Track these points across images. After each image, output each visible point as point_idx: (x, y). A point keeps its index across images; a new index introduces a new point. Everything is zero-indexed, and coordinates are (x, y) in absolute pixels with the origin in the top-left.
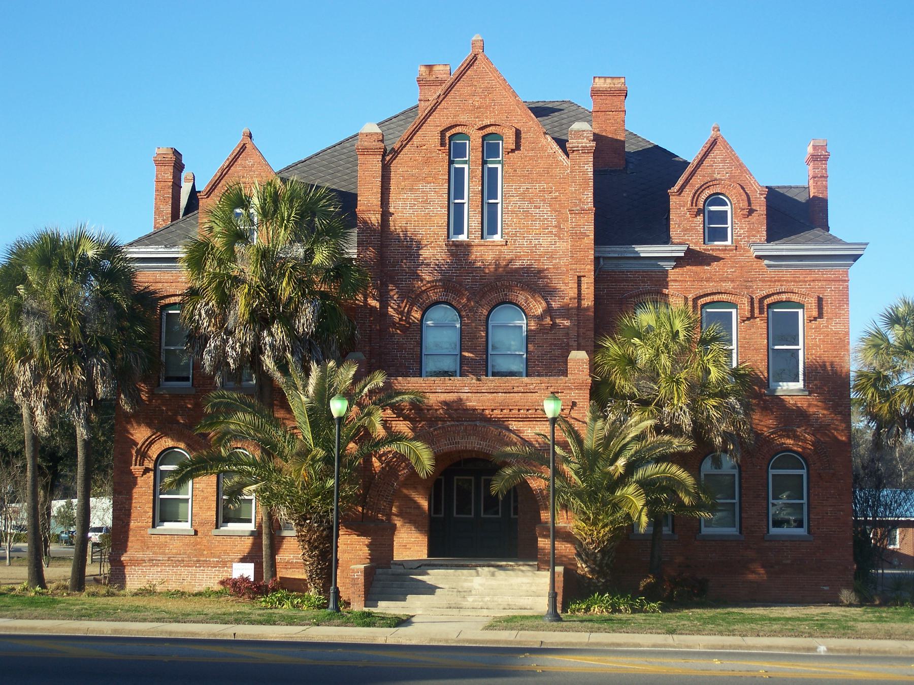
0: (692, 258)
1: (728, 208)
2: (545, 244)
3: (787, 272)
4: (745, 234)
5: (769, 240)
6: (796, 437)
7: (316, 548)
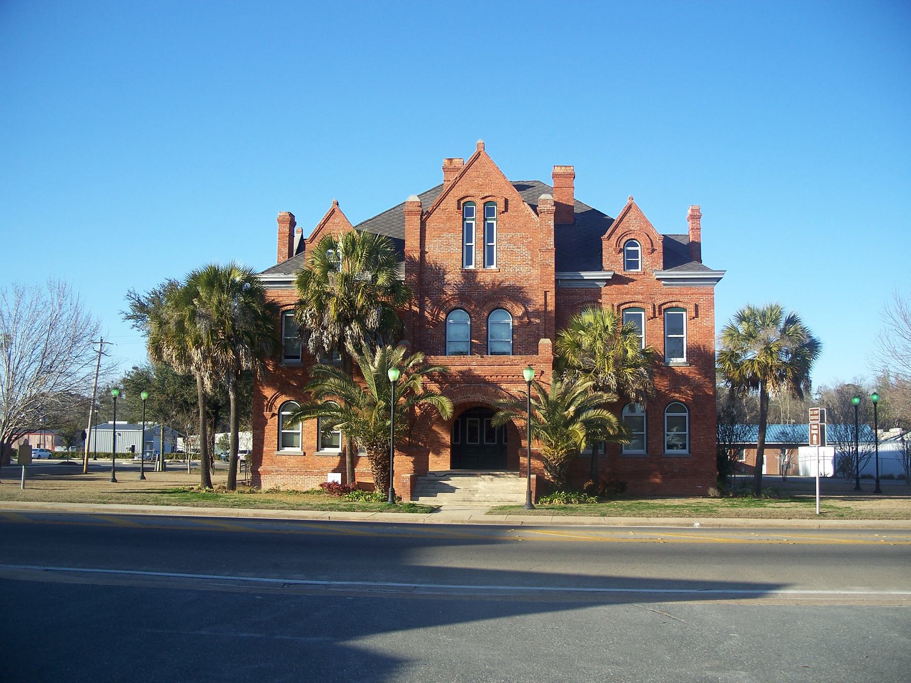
0: (617, 280)
1: (639, 248)
3: (676, 289)
4: (650, 265)
6: (680, 392)
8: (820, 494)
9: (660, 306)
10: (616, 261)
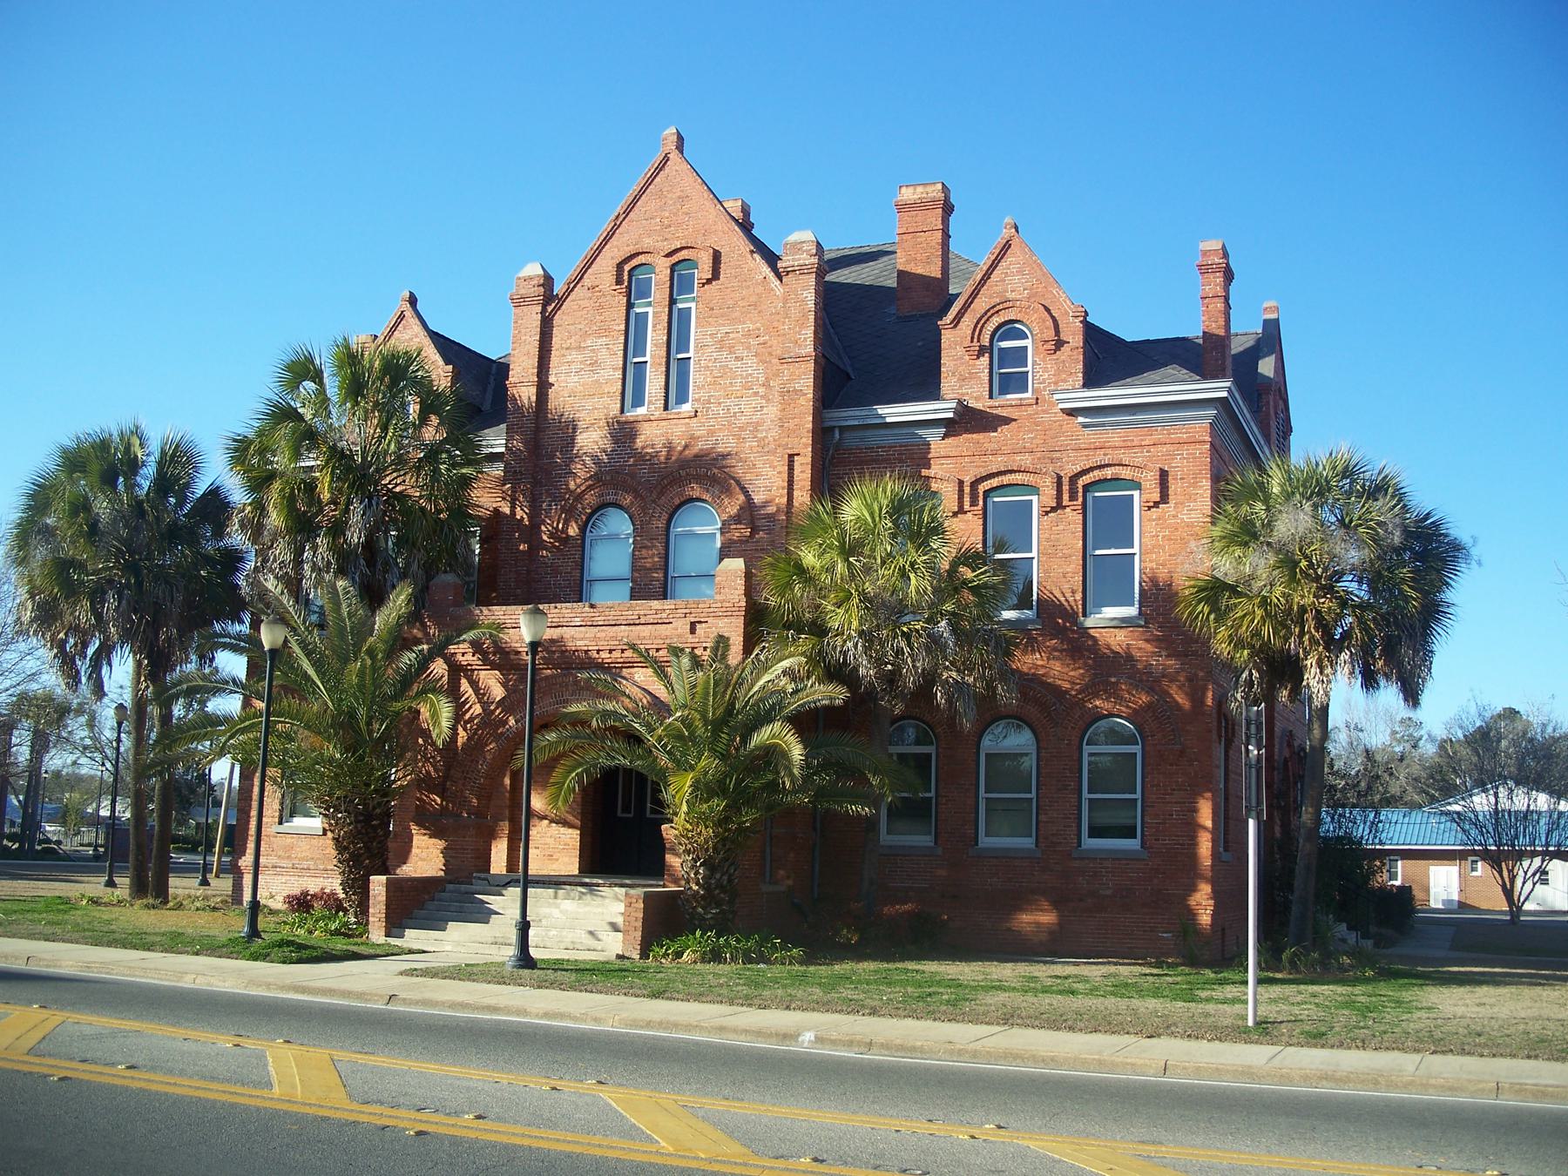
0: (967, 421)
1: (1027, 343)
2: (748, 410)
3: (1114, 434)
4: (1056, 381)
5: (1091, 381)
7: (346, 848)
8: (1259, 965)
9: (1074, 479)
10: (972, 376)
